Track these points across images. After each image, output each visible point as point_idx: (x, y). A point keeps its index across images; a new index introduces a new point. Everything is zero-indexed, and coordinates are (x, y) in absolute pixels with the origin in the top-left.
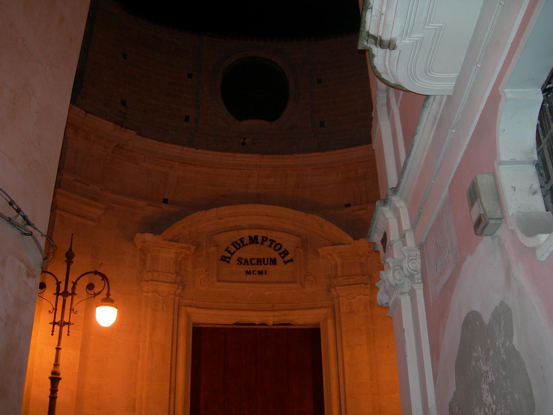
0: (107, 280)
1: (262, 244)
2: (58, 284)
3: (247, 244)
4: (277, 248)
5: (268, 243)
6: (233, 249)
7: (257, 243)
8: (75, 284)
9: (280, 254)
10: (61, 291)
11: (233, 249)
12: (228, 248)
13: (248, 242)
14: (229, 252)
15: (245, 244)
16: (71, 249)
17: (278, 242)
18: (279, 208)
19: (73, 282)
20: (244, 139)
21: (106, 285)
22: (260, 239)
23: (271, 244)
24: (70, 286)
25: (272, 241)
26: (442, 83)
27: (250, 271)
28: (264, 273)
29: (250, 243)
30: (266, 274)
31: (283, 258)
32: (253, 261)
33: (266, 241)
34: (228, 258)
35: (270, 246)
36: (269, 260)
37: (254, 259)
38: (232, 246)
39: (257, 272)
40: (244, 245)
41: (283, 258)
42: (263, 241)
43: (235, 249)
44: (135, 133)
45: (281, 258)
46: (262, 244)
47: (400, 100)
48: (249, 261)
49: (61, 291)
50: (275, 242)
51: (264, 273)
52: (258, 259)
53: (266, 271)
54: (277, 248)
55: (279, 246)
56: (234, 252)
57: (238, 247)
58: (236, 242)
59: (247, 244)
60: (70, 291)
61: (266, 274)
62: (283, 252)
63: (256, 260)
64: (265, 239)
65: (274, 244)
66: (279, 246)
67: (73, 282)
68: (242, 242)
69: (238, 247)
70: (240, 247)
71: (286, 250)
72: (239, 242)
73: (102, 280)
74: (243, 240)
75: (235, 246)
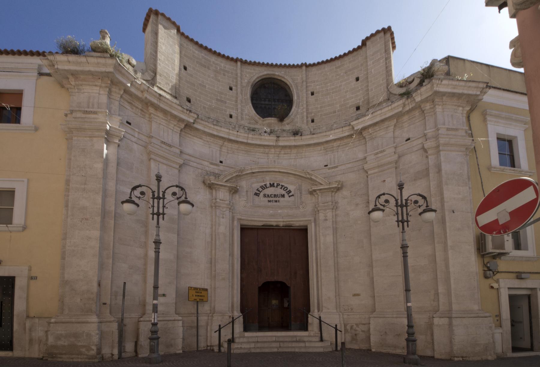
0: (185, 190)
5: (280, 187)
8: (164, 192)
10: (156, 196)
11: (261, 189)
14: (259, 191)
22: (275, 185)
25: (282, 186)
35: (281, 188)
42: (277, 186)
49: (156, 196)
60: (161, 196)
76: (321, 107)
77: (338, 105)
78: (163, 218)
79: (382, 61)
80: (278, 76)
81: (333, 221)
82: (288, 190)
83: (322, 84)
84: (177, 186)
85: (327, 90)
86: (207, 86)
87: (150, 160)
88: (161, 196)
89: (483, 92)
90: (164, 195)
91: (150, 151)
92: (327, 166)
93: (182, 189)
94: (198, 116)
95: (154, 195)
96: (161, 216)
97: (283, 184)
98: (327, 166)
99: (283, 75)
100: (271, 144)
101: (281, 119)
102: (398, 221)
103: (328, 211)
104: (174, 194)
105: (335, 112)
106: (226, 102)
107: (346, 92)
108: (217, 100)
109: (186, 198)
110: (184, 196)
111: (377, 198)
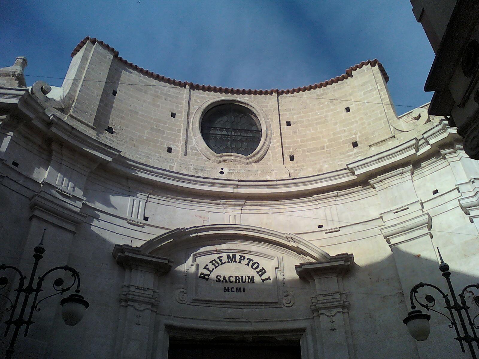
0: (78, 276)
1: (240, 262)
2: (22, 279)
3: (225, 262)
4: (254, 267)
5: (246, 261)
6: (211, 267)
7: (235, 262)
8: (41, 279)
9: (258, 272)
10: (24, 288)
11: (211, 267)
12: (207, 265)
13: (227, 260)
14: (208, 269)
15: (223, 262)
16: (387, 82)
17: (255, 261)
18: (115, 218)
19: (39, 278)
20: (222, 169)
21: (77, 278)
22: (238, 257)
23: (249, 262)
24: (36, 281)
25: (250, 260)
26: (240, 203)
27: (240, 288)
28: (242, 291)
29: (229, 262)
30: (244, 292)
31: (261, 276)
32: (231, 278)
33: (243, 260)
34: (235, 259)
35: (248, 265)
36: (247, 278)
37: (233, 277)
38: (211, 264)
39: (235, 290)
40: (222, 264)
41: (261, 276)
42: (241, 259)
43: (214, 267)
44: (5, 138)
45: (259, 276)
46: (240, 262)
47: (412, 111)
48: (230, 289)
49: (24, 288)
50: (253, 261)
51: (242, 291)
52: (236, 277)
53: (244, 288)
54: (254, 267)
55: (256, 265)
56: (213, 269)
57: (217, 265)
58: (214, 260)
59: (225, 262)
60: (35, 287)
61: (244, 292)
62: (261, 271)
63: (234, 278)
64: (242, 258)
65: (251, 263)
66: (256, 265)
67: (39, 278)
68: (221, 260)
69: (217, 265)
70: (219, 265)
71: (263, 269)
72: (218, 260)
73: (72, 276)
74: (221, 258)
75: (213, 264)
76: (302, 141)
77: (326, 140)
78: (26, 331)
79: (374, 92)
80: (241, 102)
81: (346, 332)
82: (260, 268)
83: (300, 113)
84: (66, 268)
85: (309, 120)
86: (140, 113)
87: (31, 219)
88: (35, 287)
89: (433, 125)
90: (39, 285)
91: (36, 204)
92: (322, 226)
93: (75, 274)
94: (478, 192)
95: (22, 284)
96: (23, 327)
97: (251, 257)
98: (322, 226)
99: (247, 102)
100: (375, 184)
101: (61, 304)
102: (459, 339)
103: (335, 311)
104: (59, 282)
105: (323, 148)
106: (164, 132)
107: (336, 123)
108: (152, 129)
109: (78, 291)
110: (76, 285)
111: (412, 292)
